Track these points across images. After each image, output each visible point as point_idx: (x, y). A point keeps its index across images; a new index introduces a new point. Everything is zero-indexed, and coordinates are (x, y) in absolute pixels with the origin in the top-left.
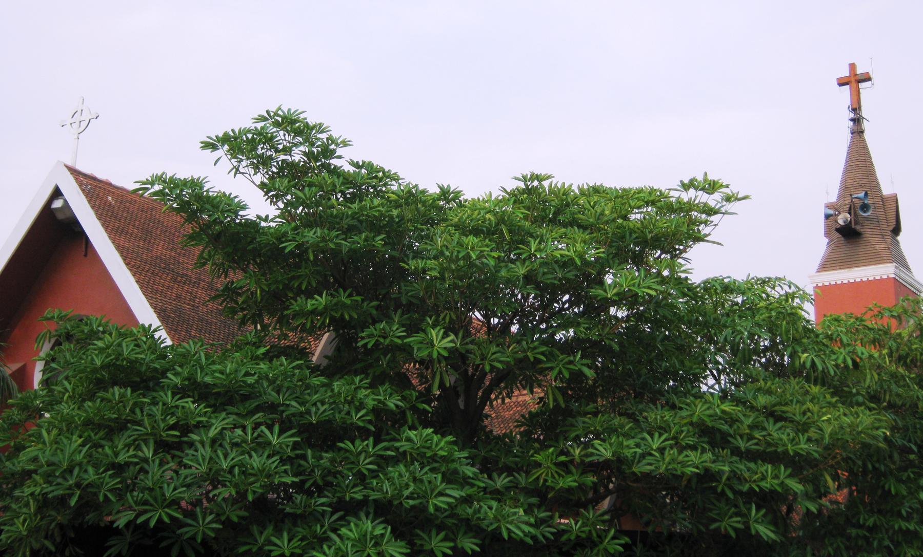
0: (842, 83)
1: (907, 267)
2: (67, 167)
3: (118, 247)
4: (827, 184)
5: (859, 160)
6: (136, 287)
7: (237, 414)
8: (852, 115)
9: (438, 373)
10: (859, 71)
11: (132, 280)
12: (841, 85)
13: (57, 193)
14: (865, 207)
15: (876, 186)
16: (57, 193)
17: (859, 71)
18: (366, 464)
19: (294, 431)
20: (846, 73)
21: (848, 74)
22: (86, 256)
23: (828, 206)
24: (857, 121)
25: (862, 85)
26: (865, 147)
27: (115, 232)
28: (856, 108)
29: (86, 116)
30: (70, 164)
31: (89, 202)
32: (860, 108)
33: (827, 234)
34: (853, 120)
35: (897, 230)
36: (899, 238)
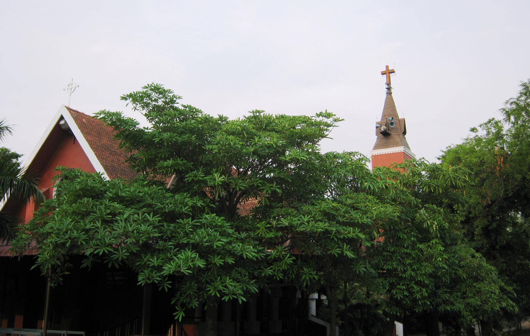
1: (409, 148)
3: (87, 140)
4: (377, 115)
5: (390, 105)
8: (387, 87)
11: (93, 153)
12: (382, 74)
13: (62, 118)
14: (392, 124)
16: (62, 118)
23: (377, 123)
24: (389, 89)
25: (391, 75)
26: (392, 99)
28: (389, 84)
29: (74, 86)
30: (67, 106)
35: (405, 133)
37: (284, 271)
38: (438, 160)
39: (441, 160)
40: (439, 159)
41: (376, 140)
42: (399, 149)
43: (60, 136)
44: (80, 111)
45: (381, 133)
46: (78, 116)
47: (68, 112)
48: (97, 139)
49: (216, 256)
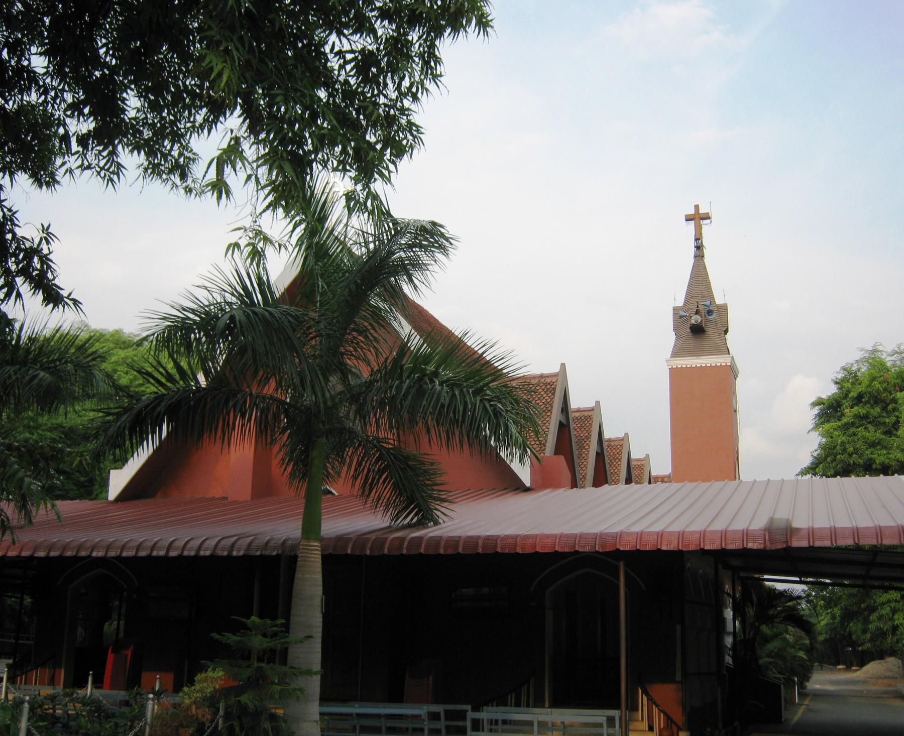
0: (689, 219)
5: (699, 278)
9: (366, 470)
19: (122, 634)
24: (699, 248)
28: (698, 239)
35: (726, 331)
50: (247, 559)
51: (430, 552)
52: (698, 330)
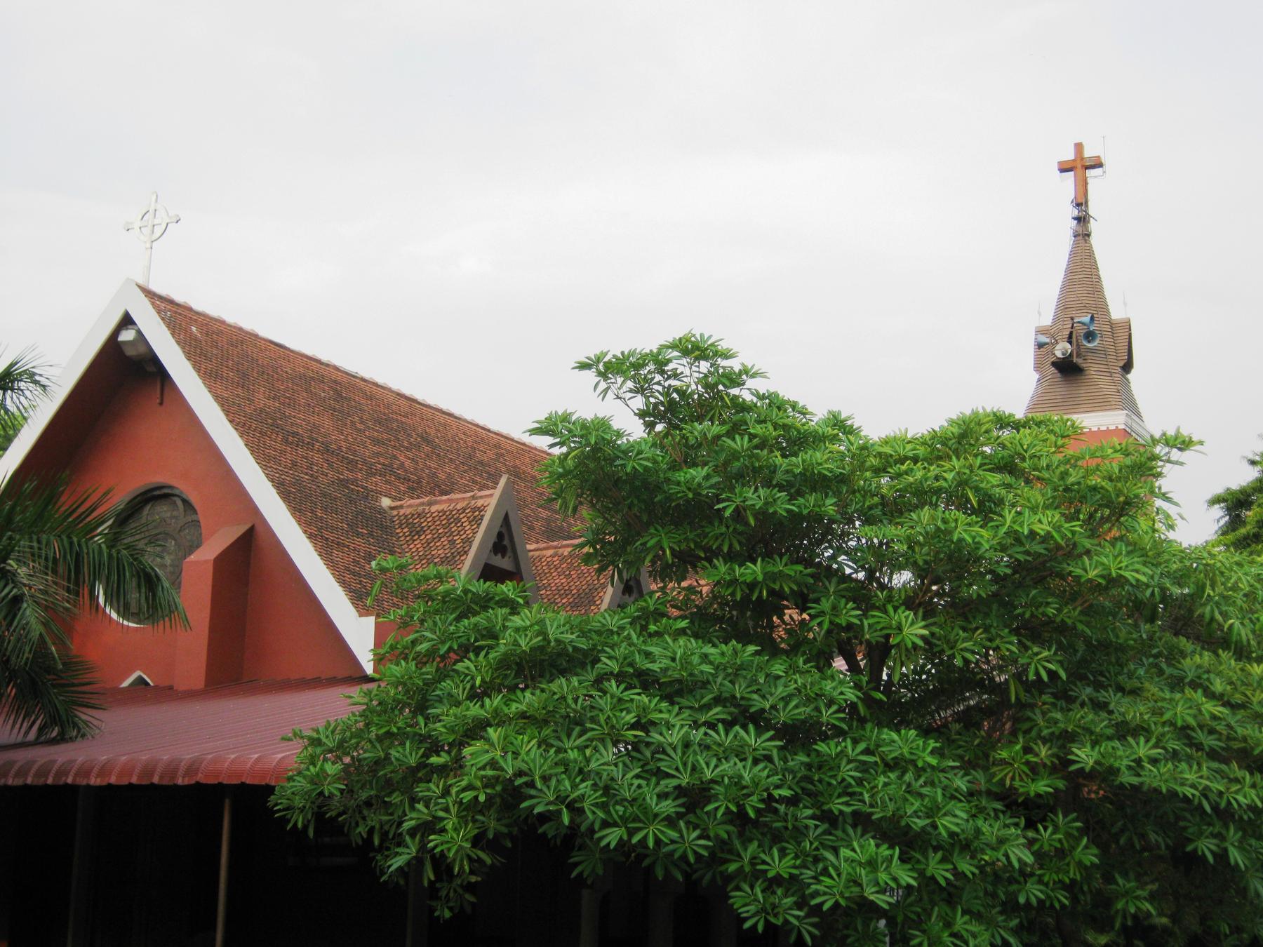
1: (1139, 415)
2: (139, 286)
3: (217, 398)
4: (1038, 300)
5: (1083, 273)
6: (246, 452)
7: (691, 708)
8: (1076, 213)
9: (399, 503)
10: (1088, 153)
11: (240, 443)
12: (1063, 170)
13: (127, 321)
14: (1090, 336)
15: (1104, 308)
16: (127, 321)
17: (1088, 153)
18: (848, 772)
20: (1069, 155)
21: (1072, 157)
22: (161, 404)
23: (1040, 331)
24: (1082, 220)
25: (1090, 173)
26: (1091, 254)
27: (210, 376)
28: (1081, 203)
29: (162, 218)
30: (141, 282)
31: (173, 335)
32: (1086, 203)
33: (1038, 367)
34: (1078, 219)
35: (1128, 367)
36: (1129, 376)
37: (1071, 887)
38: (1251, 467)
39: (1258, 468)
40: (1253, 463)
41: (1035, 384)
42: (1112, 419)
43: (122, 375)
44: (179, 298)
45: (1054, 364)
46: (177, 316)
47: (146, 302)
48: (240, 392)
49: (930, 851)
50: (200, 790)
51: (165, 782)
52: (1068, 369)
